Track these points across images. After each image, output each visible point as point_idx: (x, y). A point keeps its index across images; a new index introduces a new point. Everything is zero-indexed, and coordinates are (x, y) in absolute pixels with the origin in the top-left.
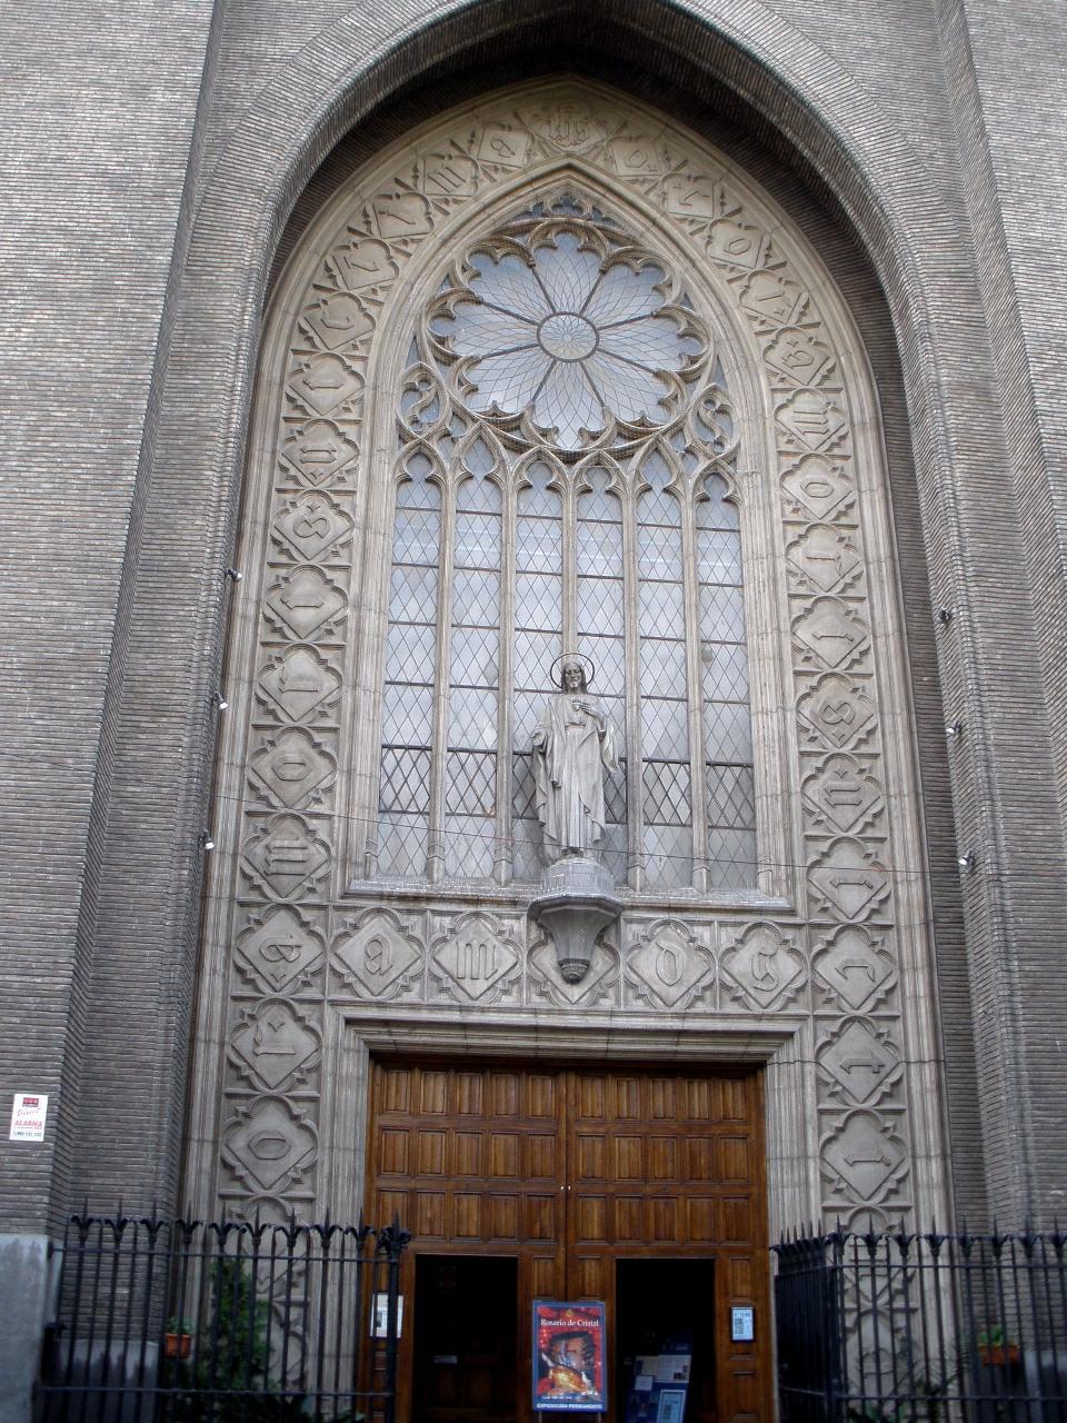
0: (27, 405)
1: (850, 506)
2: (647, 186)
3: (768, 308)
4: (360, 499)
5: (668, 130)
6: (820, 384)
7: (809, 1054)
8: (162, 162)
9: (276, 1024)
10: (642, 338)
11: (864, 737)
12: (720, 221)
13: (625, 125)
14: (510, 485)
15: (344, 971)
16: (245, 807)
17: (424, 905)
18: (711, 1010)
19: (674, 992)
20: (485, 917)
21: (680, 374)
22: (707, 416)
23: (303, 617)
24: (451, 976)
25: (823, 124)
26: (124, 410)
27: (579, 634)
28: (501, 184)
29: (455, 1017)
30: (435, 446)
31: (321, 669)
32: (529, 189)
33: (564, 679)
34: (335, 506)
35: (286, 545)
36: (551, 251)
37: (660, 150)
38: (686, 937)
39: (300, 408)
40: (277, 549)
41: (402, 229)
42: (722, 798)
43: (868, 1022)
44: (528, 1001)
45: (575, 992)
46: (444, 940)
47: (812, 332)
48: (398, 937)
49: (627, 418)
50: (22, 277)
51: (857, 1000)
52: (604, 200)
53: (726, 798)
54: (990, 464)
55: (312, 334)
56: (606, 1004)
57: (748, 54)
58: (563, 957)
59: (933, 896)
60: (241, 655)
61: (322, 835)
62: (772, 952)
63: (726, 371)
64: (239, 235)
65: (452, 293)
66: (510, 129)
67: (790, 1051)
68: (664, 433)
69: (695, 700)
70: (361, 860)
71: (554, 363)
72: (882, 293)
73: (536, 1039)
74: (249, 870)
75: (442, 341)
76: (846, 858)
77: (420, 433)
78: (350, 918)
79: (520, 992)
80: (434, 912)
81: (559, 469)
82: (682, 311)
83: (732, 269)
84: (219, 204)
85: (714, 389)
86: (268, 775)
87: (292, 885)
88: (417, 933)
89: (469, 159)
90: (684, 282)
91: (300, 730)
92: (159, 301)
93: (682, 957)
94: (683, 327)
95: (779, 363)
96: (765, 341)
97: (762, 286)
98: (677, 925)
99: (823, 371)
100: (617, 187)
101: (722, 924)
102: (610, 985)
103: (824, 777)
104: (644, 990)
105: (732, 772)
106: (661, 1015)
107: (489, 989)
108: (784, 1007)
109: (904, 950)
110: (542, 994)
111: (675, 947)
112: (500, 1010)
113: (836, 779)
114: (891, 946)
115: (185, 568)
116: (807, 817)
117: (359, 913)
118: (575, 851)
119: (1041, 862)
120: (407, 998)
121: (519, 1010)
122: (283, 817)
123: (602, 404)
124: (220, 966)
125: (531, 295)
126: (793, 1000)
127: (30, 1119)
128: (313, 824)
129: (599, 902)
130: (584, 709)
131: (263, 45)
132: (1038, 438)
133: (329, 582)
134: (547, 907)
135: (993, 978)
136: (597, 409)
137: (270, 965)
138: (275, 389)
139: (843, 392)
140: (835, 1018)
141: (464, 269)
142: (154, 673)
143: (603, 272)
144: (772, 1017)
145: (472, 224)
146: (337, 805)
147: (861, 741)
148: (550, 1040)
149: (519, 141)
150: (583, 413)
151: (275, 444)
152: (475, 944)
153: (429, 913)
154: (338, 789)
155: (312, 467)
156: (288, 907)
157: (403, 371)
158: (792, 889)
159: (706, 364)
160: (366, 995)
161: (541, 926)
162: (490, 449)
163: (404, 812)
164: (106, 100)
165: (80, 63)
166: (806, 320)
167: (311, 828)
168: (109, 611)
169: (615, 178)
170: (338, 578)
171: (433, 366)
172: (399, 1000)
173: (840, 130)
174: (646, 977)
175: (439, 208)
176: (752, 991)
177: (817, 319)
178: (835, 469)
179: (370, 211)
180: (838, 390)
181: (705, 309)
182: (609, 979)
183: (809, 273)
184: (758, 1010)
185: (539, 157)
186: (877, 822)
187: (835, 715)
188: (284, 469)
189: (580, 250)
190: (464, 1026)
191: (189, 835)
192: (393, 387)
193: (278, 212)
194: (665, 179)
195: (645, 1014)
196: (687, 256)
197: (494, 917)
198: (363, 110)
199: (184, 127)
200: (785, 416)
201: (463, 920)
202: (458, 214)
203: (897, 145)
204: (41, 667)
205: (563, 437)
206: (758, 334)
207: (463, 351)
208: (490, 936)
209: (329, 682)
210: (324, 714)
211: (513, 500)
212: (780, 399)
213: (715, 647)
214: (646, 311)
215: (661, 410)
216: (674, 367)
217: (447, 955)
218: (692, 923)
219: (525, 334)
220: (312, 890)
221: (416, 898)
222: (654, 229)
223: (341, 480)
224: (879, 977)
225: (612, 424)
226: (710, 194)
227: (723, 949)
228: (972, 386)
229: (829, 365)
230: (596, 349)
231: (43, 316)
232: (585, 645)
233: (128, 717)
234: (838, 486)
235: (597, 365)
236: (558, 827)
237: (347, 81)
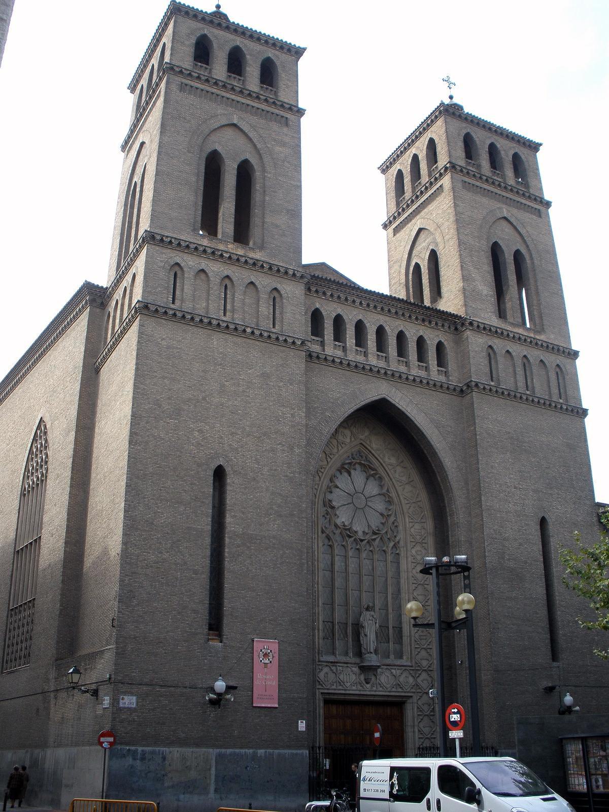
7: (415, 701)
15: (320, 681)
17: (336, 664)
18: (396, 690)
29: (343, 692)
45: (368, 686)
50: (271, 508)
57: (419, 429)
67: (410, 701)
76: (423, 653)
80: (339, 666)
106: (386, 691)
111: (388, 675)
127: (302, 726)
140: (421, 692)
144: (408, 692)
164: (283, 450)
173: (442, 460)
180: (424, 522)
184: (405, 691)
196: (389, 476)
215: (382, 525)
221: (334, 662)
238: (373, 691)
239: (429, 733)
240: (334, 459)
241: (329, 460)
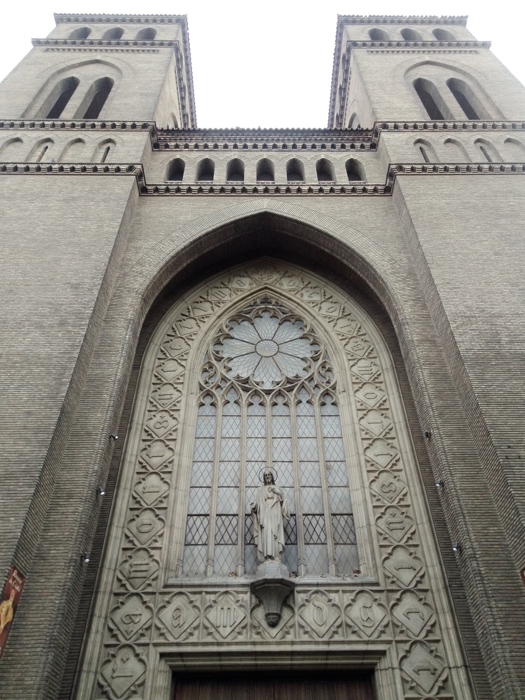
0: (22, 367)
1: (385, 401)
2: (295, 292)
3: (345, 330)
4: (182, 412)
5: (303, 272)
6: (368, 356)
8: (93, 278)
9: (125, 659)
10: (296, 346)
11: (402, 497)
12: (324, 301)
13: (286, 272)
14: (244, 402)
16: (123, 546)
18: (342, 639)
19: (323, 629)
20: (230, 593)
21: (311, 358)
22: (323, 372)
23: (156, 461)
24: (213, 626)
25: (357, 254)
26: (65, 368)
27: (273, 462)
28: (240, 295)
30: (213, 391)
31: (161, 482)
32: (251, 297)
33: (264, 479)
34: (171, 416)
35: (150, 432)
36: (260, 318)
37: (300, 279)
38: (327, 599)
39: (159, 379)
40: (147, 434)
41: (202, 313)
42: (340, 530)
43: (424, 644)
44: (251, 637)
45: (274, 632)
46: (211, 606)
47: (363, 337)
48: (190, 606)
49: (291, 376)
51: (417, 632)
52: (279, 299)
53: (342, 529)
54: (440, 369)
55: (166, 352)
56: (290, 638)
58: (267, 612)
59: (447, 573)
60: (127, 479)
61: (156, 558)
62: (369, 606)
63: (329, 355)
64: (127, 307)
65: (221, 335)
66: (243, 276)
67: (384, 663)
68: (306, 380)
69: (324, 486)
70: (174, 568)
71: (261, 358)
72: (390, 320)
73: (256, 660)
74: (121, 577)
75: (218, 352)
76: (401, 556)
77: (208, 387)
78: (167, 598)
79: (247, 633)
81: (263, 396)
82: (311, 335)
83: (329, 318)
84: (120, 297)
85: (325, 362)
86: (135, 530)
87: (141, 582)
88: (198, 604)
89: (228, 288)
90: (311, 324)
91: (151, 509)
92: (86, 327)
93: (326, 609)
94: (312, 340)
95: (351, 350)
96: (344, 342)
97: (342, 322)
98: (322, 593)
99: (369, 351)
100: (284, 293)
101: (344, 592)
102: (291, 627)
103: (385, 517)
104: (308, 629)
105: (344, 518)
106: (317, 643)
107: (231, 632)
108: (379, 636)
109: (437, 602)
110: (258, 633)
112: (237, 644)
113: (391, 518)
114: (430, 601)
115: (89, 434)
116: (380, 536)
117: (171, 595)
118: (271, 557)
119: (496, 546)
120: (191, 640)
121: (246, 643)
122: (139, 550)
123: (281, 371)
124: (101, 628)
125: (253, 335)
126: (383, 632)
128: (153, 552)
129: (281, 581)
130: (273, 491)
131: (139, 244)
132: (458, 353)
133: (167, 446)
134: (257, 586)
135: (482, 612)
136: (279, 373)
137: (125, 626)
138: (150, 373)
139: (377, 358)
140: (406, 642)
141: (226, 327)
142: (70, 479)
143: (280, 324)
144: (374, 642)
145: (229, 310)
146: (164, 543)
147: (401, 500)
148: (263, 660)
149: (246, 281)
150: (274, 375)
151: (148, 392)
152: (226, 608)
153: (204, 593)
154: (165, 535)
155: (163, 401)
156: (137, 594)
157: (202, 364)
158: (376, 571)
159: (321, 353)
160: (171, 640)
161: (257, 597)
162: (236, 391)
163: (196, 545)
165: (65, 247)
166: (360, 333)
167: (151, 554)
168: (44, 449)
169: (283, 290)
170: (171, 444)
171: (214, 362)
172: (187, 641)
174: (308, 621)
175: (216, 305)
176: (362, 627)
177: (364, 332)
178: (377, 387)
179: (190, 308)
181: (320, 334)
182: (290, 623)
183: (361, 317)
185: (255, 285)
186: (413, 537)
187: (387, 489)
188: (151, 403)
189: (271, 317)
190: (220, 654)
191: (74, 555)
192: (198, 369)
193: (145, 300)
194: (302, 289)
195: (309, 643)
196: (312, 315)
197: (234, 593)
198: (182, 267)
199: (103, 267)
200: (354, 369)
201: (220, 596)
202: (223, 307)
203: (387, 258)
204: (7, 476)
205: (266, 385)
206: (341, 340)
207: (226, 356)
208: (232, 603)
209: (165, 487)
210: (161, 502)
211: (245, 408)
212: (352, 363)
213: (332, 463)
214: (297, 336)
215: (305, 372)
216: (309, 356)
217: (212, 615)
218: (329, 591)
219: (251, 348)
220: (149, 585)
222: (299, 307)
223: (175, 405)
224: (426, 618)
225: (284, 378)
226: (319, 292)
227: (345, 605)
228: (427, 340)
229: (371, 348)
230: (278, 352)
231: (36, 334)
232: (276, 466)
233: (54, 500)
234: (379, 394)
235: (278, 358)
236: (263, 546)
237: (173, 254)
238: (286, 643)
239: (432, 688)
240: (189, 361)
241: (183, 363)
